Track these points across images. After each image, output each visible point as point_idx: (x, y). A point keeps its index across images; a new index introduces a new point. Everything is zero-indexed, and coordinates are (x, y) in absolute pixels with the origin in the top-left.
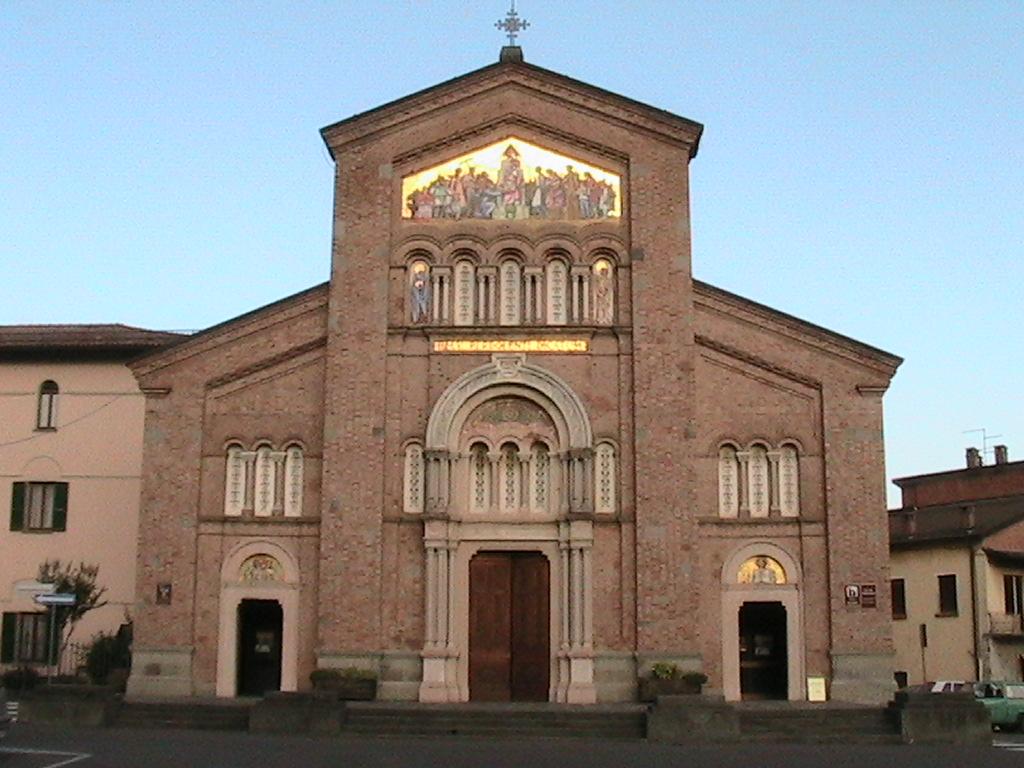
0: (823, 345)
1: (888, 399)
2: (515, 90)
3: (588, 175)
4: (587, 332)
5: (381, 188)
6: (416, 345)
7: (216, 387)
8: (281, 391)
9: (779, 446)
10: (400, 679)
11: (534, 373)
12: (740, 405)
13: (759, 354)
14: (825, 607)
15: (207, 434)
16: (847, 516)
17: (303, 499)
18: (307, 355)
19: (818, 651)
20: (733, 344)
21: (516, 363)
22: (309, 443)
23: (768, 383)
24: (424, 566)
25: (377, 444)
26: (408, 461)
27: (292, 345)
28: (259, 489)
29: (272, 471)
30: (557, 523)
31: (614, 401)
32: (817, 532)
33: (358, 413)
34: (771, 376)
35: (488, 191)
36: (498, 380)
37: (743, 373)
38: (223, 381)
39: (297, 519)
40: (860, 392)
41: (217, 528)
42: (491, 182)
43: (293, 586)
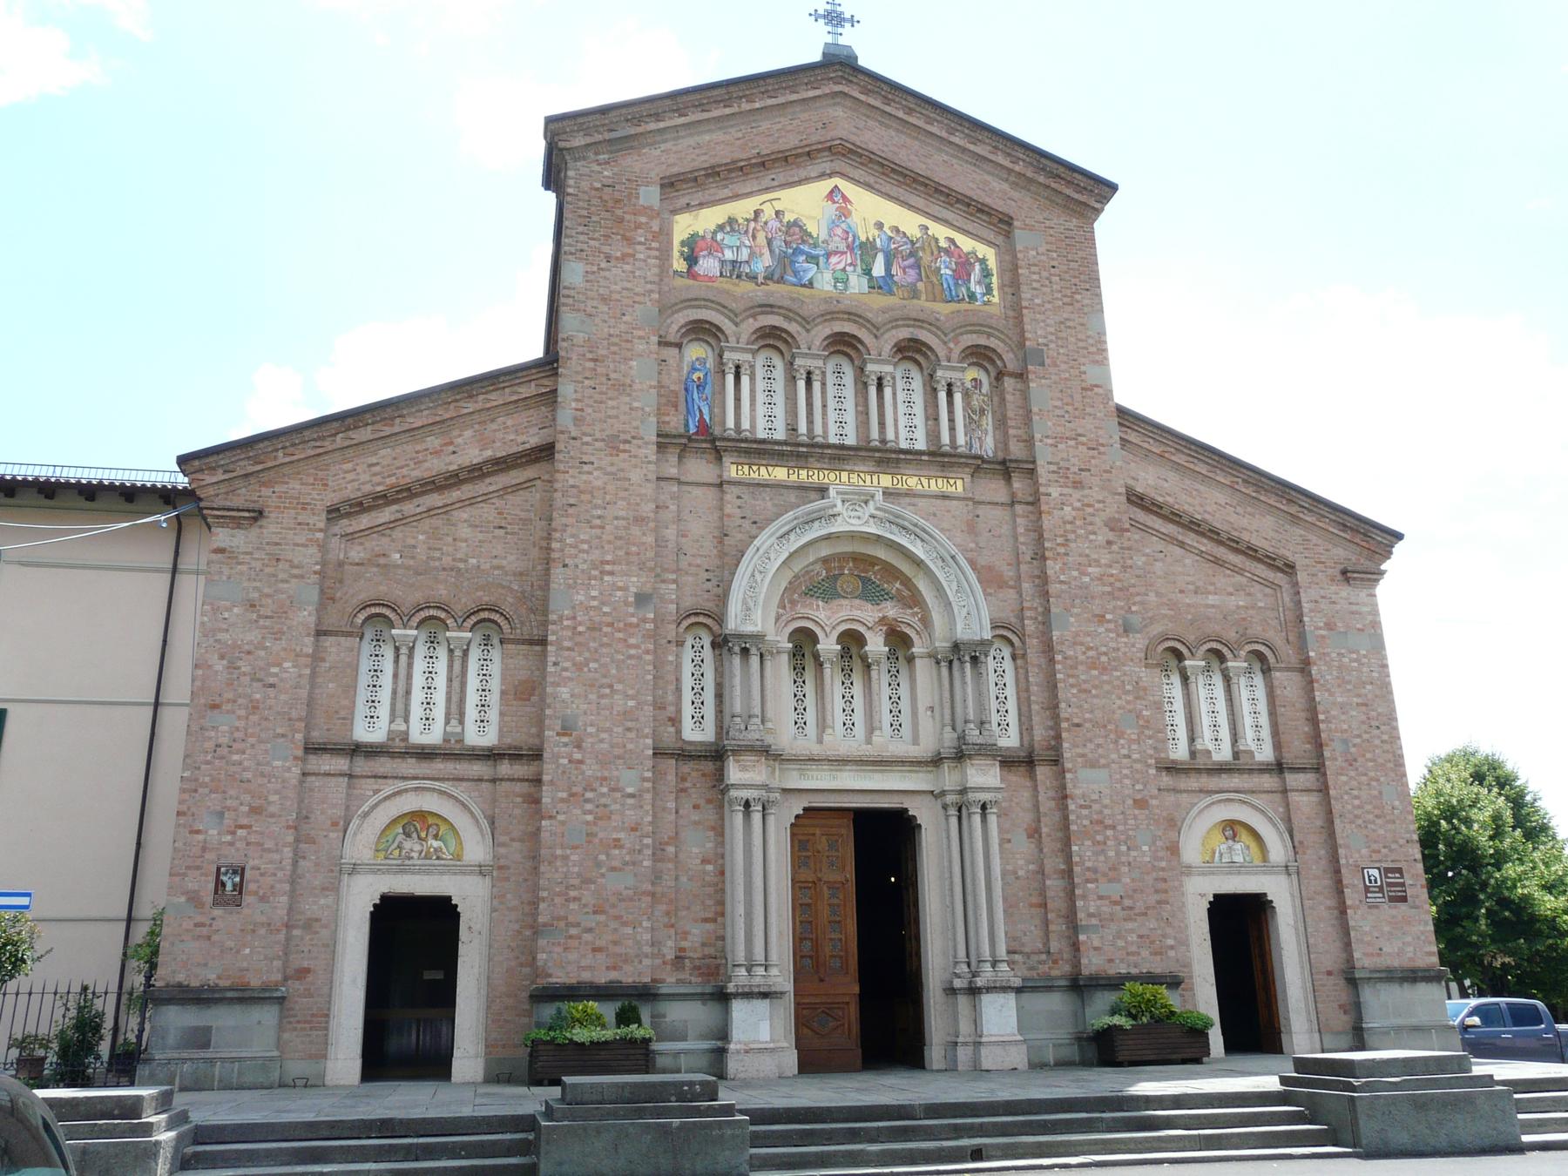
0: (1293, 509)
1: (1383, 590)
2: (833, 108)
3: (952, 241)
4: (967, 465)
5: (643, 220)
6: (699, 468)
7: (348, 515)
8: (465, 531)
9: (1243, 653)
10: (684, 1039)
11: (896, 522)
12: (1182, 592)
13: (1207, 516)
14: (1331, 903)
15: (326, 598)
16: (1351, 762)
17: (502, 714)
18: (513, 473)
19: (1329, 973)
20: (1170, 500)
21: (866, 502)
22: (515, 622)
23: (1217, 561)
24: (720, 831)
25: (644, 620)
26: (688, 654)
27: (488, 453)
28: (417, 696)
29: (441, 666)
30: (936, 761)
31: (1009, 573)
32: (1308, 785)
33: (608, 568)
34: (1221, 552)
35: (806, 248)
36: (838, 527)
37: (1182, 545)
38: (360, 506)
39: (490, 749)
40: (1347, 580)
41: (341, 764)
42: (810, 235)
43: (481, 871)
